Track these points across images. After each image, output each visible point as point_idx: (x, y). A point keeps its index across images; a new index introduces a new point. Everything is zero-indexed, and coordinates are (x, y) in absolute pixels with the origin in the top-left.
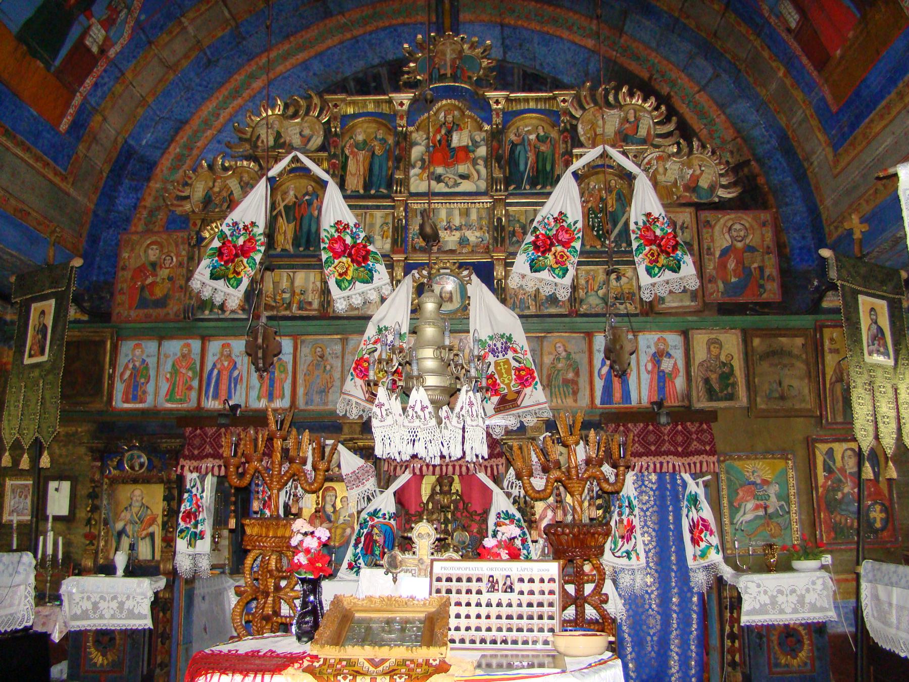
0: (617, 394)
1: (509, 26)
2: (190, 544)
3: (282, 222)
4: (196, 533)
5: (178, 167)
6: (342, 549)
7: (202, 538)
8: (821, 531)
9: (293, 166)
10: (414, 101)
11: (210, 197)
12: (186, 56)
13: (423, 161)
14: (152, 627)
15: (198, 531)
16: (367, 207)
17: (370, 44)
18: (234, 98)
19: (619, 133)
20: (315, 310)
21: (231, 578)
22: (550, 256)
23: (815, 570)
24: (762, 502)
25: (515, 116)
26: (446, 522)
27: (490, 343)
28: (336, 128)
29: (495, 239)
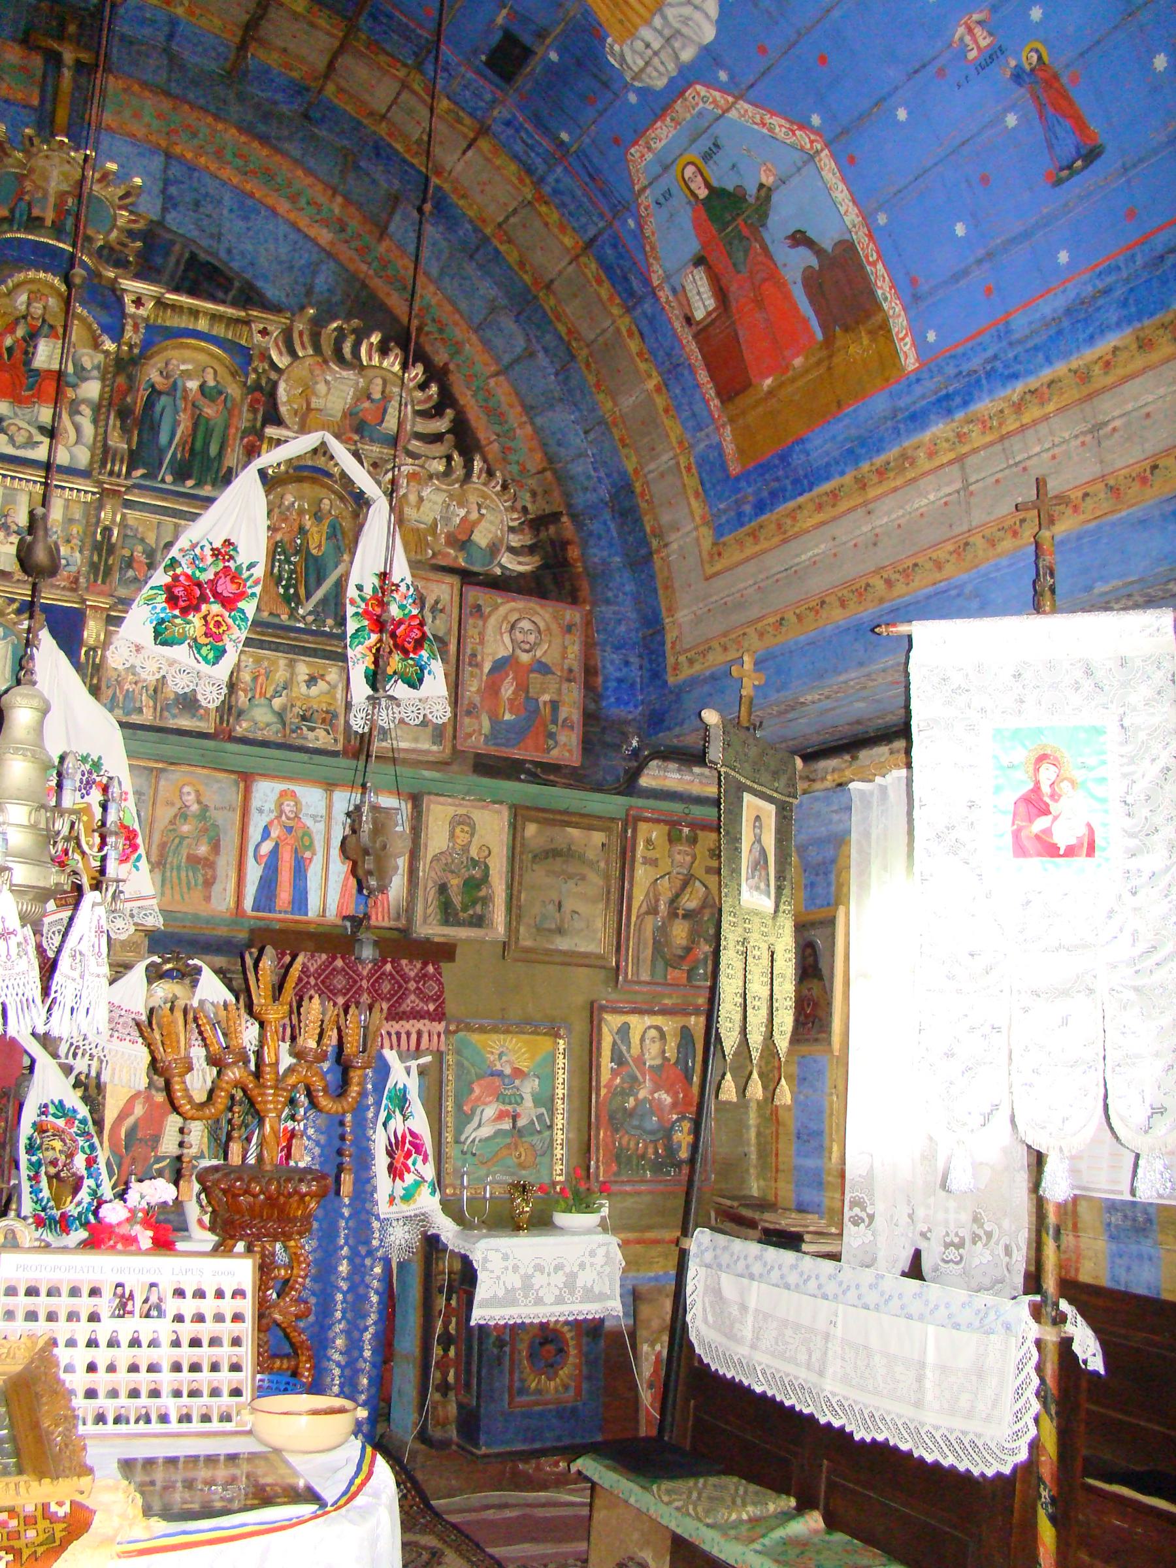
0: (284, 894)
1: (180, 159)
8: (597, 1161)
19: (349, 414)
22: (196, 620)
23: (589, 1232)
24: (509, 1108)
25: (169, 338)
29: (94, 567)
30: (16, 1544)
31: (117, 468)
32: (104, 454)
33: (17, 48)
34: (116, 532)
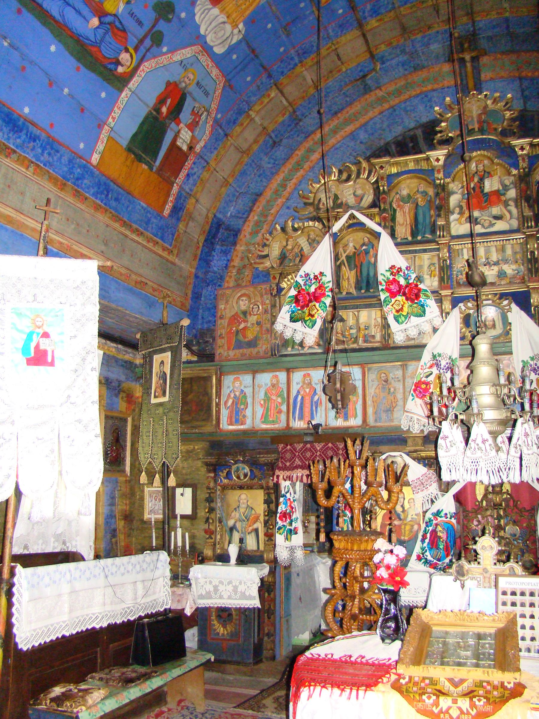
2: (287, 539)
3: (345, 270)
4: (291, 530)
5: (257, 232)
6: (410, 543)
7: (296, 533)
9: (351, 222)
10: (448, 156)
11: (284, 254)
12: (256, 141)
13: (461, 207)
14: (260, 606)
15: (292, 528)
16: (415, 251)
17: (406, 111)
18: (297, 170)
20: (379, 342)
21: (319, 556)
26: (499, 518)
27: (532, 363)
28: (383, 186)
29: (530, 271)
30: (488, 696)
31: (529, 224)
32: (523, 219)
33: (446, 64)
34: (536, 253)
